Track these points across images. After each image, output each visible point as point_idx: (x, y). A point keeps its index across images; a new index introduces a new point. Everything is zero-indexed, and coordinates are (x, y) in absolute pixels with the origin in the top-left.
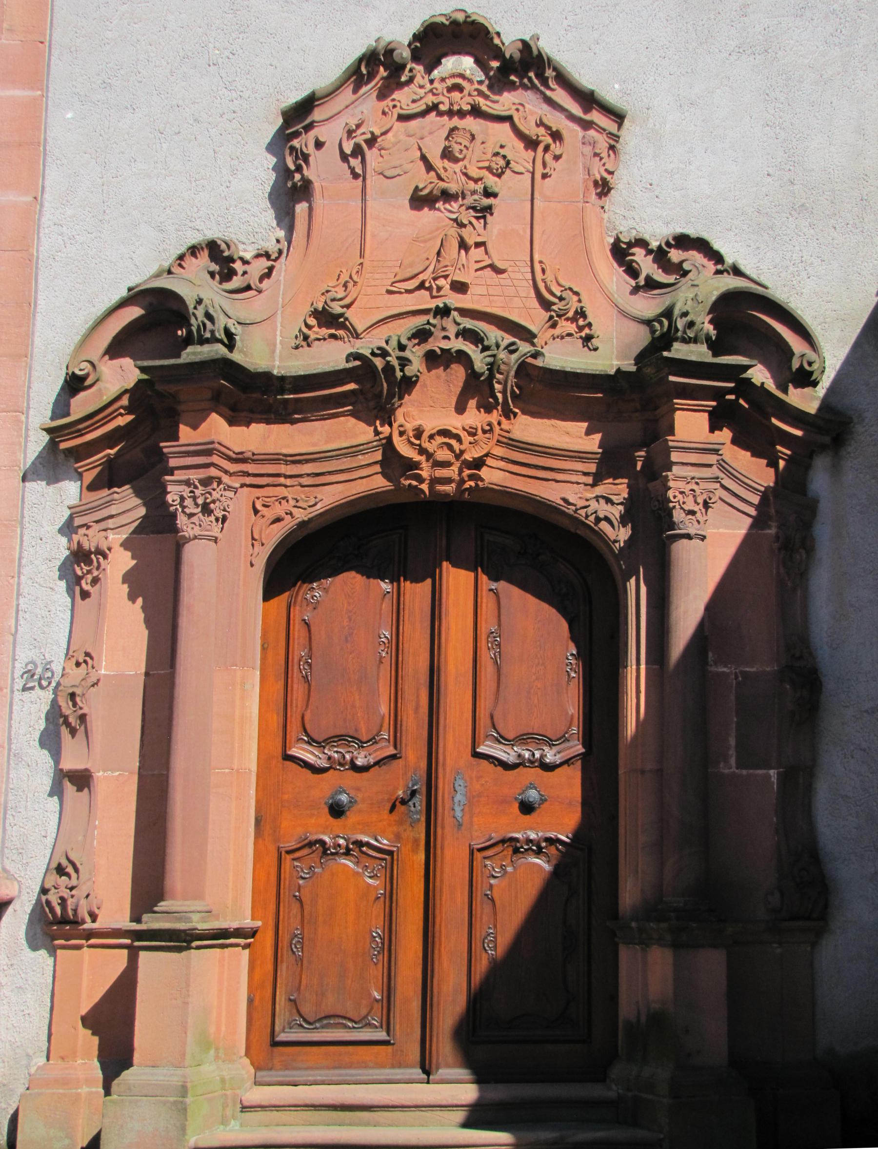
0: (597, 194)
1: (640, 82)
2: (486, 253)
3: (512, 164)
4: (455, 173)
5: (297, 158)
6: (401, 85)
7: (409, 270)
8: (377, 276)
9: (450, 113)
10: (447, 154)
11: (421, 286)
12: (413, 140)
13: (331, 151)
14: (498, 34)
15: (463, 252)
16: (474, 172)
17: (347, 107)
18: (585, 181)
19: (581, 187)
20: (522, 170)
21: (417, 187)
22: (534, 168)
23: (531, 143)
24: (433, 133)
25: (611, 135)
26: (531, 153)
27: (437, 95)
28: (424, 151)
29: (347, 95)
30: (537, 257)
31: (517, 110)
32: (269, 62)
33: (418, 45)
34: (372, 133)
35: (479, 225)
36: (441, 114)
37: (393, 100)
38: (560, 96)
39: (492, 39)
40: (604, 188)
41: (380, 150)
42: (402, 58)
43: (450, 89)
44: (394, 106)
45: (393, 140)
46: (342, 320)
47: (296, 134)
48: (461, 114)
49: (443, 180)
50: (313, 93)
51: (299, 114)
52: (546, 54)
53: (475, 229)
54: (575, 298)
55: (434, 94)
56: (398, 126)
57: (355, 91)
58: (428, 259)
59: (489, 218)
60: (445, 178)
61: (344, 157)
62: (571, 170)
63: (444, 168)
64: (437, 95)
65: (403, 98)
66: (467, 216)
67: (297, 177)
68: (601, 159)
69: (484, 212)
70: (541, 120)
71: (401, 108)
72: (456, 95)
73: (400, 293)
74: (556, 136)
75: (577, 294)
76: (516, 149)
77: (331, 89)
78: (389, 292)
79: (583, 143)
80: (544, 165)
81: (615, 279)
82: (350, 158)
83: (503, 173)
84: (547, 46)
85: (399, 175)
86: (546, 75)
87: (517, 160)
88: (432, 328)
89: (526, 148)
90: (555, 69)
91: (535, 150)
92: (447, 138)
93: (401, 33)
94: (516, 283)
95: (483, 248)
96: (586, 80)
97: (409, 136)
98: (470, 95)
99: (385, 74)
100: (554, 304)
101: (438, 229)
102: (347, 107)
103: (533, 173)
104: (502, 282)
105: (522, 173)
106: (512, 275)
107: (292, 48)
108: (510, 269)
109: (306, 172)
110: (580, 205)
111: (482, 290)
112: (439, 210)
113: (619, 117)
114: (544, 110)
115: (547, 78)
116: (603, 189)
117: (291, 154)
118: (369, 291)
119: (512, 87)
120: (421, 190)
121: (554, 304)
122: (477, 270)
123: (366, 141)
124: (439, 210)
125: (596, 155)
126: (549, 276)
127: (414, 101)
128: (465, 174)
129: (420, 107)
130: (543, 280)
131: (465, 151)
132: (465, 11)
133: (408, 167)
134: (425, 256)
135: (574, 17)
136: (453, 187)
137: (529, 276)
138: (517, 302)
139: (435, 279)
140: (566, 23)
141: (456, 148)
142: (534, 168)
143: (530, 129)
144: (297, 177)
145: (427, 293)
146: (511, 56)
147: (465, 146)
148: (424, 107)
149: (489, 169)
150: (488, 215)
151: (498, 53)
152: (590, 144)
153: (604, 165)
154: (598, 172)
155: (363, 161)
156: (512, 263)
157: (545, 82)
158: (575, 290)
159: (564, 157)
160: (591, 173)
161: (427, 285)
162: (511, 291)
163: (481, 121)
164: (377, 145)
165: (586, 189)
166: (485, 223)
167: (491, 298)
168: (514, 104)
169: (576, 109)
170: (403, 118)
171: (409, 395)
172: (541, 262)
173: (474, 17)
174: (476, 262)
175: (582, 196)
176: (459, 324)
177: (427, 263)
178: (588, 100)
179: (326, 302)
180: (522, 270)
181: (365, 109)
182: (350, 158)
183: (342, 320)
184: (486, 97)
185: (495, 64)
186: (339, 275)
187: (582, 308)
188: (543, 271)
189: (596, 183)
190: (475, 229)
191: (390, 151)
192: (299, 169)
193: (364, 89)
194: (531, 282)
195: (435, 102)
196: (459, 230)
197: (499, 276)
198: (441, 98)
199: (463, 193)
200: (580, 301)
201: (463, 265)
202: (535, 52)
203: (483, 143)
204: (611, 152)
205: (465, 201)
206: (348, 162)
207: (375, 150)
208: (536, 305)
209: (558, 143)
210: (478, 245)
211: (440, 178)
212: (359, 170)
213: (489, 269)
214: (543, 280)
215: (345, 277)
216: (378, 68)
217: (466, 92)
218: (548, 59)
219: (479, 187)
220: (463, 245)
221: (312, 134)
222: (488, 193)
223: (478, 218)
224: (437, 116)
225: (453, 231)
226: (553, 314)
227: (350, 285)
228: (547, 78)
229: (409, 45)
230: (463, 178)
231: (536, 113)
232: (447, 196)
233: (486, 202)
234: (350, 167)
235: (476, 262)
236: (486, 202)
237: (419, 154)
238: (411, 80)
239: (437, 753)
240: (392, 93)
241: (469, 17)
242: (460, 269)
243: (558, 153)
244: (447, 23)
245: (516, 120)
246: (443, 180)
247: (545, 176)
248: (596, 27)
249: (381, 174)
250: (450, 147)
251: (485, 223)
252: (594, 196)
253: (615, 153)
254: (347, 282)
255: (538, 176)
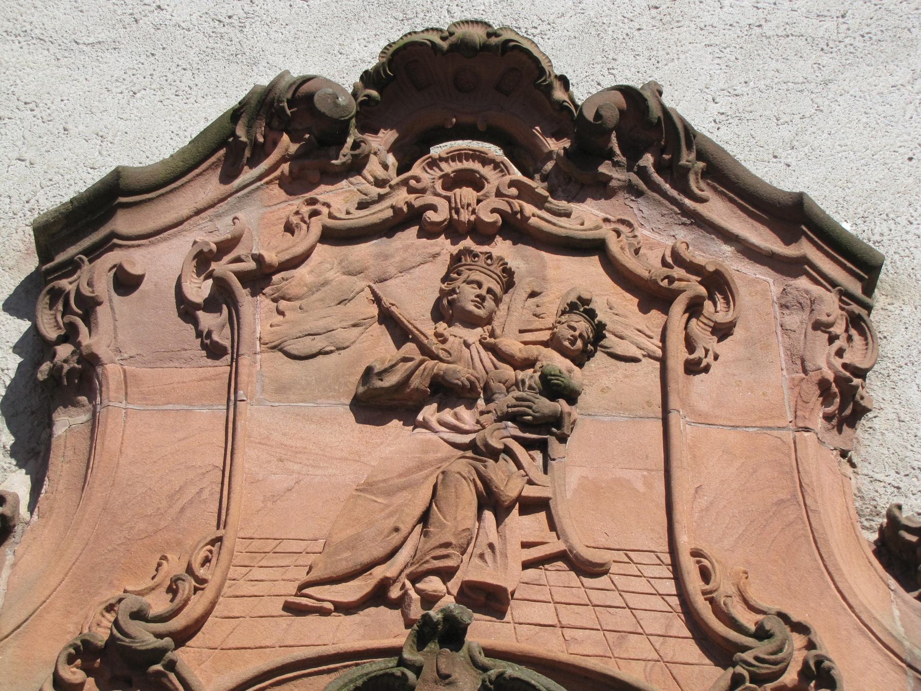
0: (828, 418)
1: (903, 220)
2: (552, 526)
3: (610, 340)
4: (467, 345)
5: (67, 310)
6: (333, 176)
7: (347, 554)
8: (257, 573)
9: (453, 230)
10: (446, 310)
11: (379, 596)
12: (360, 283)
13: (154, 306)
14: (564, 82)
15: (489, 515)
16: (512, 344)
17: (198, 212)
18: (795, 385)
19: (788, 398)
20: (634, 352)
21: (369, 371)
22: (664, 348)
23: (653, 296)
24: (414, 274)
25: (845, 295)
26: (656, 316)
27: (423, 191)
28: (386, 301)
29: (208, 187)
30: (685, 542)
31: (618, 233)
32: (16, 155)
33: (374, 93)
34: (258, 259)
35: (532, 461)
36: (429, 232)
37: (312, 201)
38: (717, 209)
39: (550, 87)
40: (845, 402)
41: (275, 300)
42: (337, 105)
43: (452, 182)
44: (315, 213)
45: (309, 279)
46: (158, 667)
47: (71, 267)
48: (482, 233)
49: (434, 357)
50: (117, 174)
51: (84, 224)
52: (682, 120)
53: (519, 466)
54: (798, 640)
55: (411, 190)
56: (322, 251)
57: (226, 178)
58: (397, 530)
59: (555, 446)
60: (442, 354)
61: (187, 310)
62: (757, 365)
63: (437, 335)
64: (423, 191)
65: (339, 200)
66: (502, 435)
67: (64, 351)
68: (832, 339)
69: (543, 431)
70: (675, 254)
71: (331, 216)
72: (467, 194)
73: (324, 612)
74: (717, 283)
75: (801, 628)
76: (616, 306)
77: (162, 175)
78: (293, 609)
79: (784, 306)
80: (690, 345)
81: (897, 613)
82: (200, 314)
83: (590, 355)
84: (687, 103)
85: (321, 353)
86: (683, 162)
87: (620, 329)
88: (411, 675)
89: (644, 308)
90: (701, 156)
91: (665, 308)
92: (446, 279)
93: (342, 62)
94: (633, 601)
95: (542, 515)
96: (779, 176)
97: (350, 274)
98: (499, 194)
99: (294, 148)
100: (745, 649)
101: (421, 466)
102: (198, 212)
103: (663, 361)
104: (597, 597)
105: (635, 360)
106: (621, 582)
107: (73, 131)
108: (614, 568)
109: (84, 338)
110: (788, 436)
111: (545, 614)
112: (425, 425)
113: (866, 266)
114: (684, 237)
115: (686, 170)
116: (842, 408)
117: (52, 305)
118: (237, 607)
119: (601, 189)
120: (381, 375)
121: (745, 649)
122: (526, 565)
123: (243, 277)
124: (425, 425)
125: (818, 326)
126: (724, 586)
127: (362, 206)
128: (492, 349)
129: (381, 212)
130: (704, 593)
131: (489, 303)
132: (487, 25)
133: (345, 335)
134: (391, 523)
135: (732, 99)
136: (461, 372)
137: (670, 587)
138: (638, 646)
139: (415, 578)
140: (714, 109)
141: (467, 295)
142: (664, 348)
143: (648, 265)
144: (64, 351)
145: (395, 615)
146: (598, 116)
147: (490, 291)
148: (389, 213)
149: (553, 343)
150: (553, 441)
151: (565, 119)
152: (802, 306)
153: (840, 353)
154: (825, 362)
155: (235, 321)
156: (621, 556)
157: (676, 174)
158: (795, 617)
159: (738, 331)
160: (809, 365)
161: (395, 593)
162: (623, 620)
163: (530, 250)
164: (267, 290)
165: (800, 401)
166: (546, 458)
167: (567, 632)
168: (606, 220)
169: (762, 237)
170: (331, 236)
171: (404, 425)
172: (696, 553)
173: (507, 35)
174: (525, 545)
175: (790, 417)
176: (485, 669)
177: (396, 538)
178: (793, 216)
179: (116, 623)
180: (649, 571)
181: (262, 218)
182: (200, 314)
183: (158, 667)
184: (539, 202)
185: (555, 146)
186: (159, 565)
187: (819, 662)
188: (705, 575)
189: (824, 385)
190: (519, 466)
191: (303, 302)
192: (70, 335)
193: (248, 174)
194: (675, 601)
195: (417, 204)
196: (480, 465)
197: (588, 582)
198: (429, 199)
199: (487, 388)
200: (811, 646)
201: (491, 546)
202: (656, 112)
203: (533, 295)
204: (853, 332)
205: (492, 406)
206: (195, 322)
207: (264, 302)
208: (692, 651)
209: (719, 297)
210: (529, 506)
211: (425, 351)
212: (222, 338)
213: (560, 564)
214: (704, 593)
215: (174, 566)
216: (283, 131)
217: (490, 188)
218: (687, 129)
219: (530, 376)
220: (490, 501)
221: (111, 258)
222: (554, 388)
223: (528, 445)
224: (420, 236)
225: (462, 466)
226: (739, 669)
227: (188, 584)
228: (686, 170)
229: (355, 95)
230: (487, 357)
231: (659, 244)
232: (446, 392)
233: (545, 405)
234: (199, 334)
235: (525, 545)
236: (545, 405)
237: (374, 310)
238: (356, 166)
239: (819, 248)
240: (314, 185)
241: (496, 34)
242: (482, 556)
243: (722, 317)
244: (445, 45)
245: (614, 246)
246: (434, 357)
247: (693, 368)
248: (785, 118)
249: (277, 347)
250: (453, 291)
251: (546, 458)
252: (819, 423)
253: (862, 333)
254: (176, 580)
255: (676, 364)
